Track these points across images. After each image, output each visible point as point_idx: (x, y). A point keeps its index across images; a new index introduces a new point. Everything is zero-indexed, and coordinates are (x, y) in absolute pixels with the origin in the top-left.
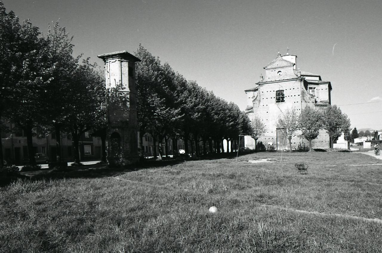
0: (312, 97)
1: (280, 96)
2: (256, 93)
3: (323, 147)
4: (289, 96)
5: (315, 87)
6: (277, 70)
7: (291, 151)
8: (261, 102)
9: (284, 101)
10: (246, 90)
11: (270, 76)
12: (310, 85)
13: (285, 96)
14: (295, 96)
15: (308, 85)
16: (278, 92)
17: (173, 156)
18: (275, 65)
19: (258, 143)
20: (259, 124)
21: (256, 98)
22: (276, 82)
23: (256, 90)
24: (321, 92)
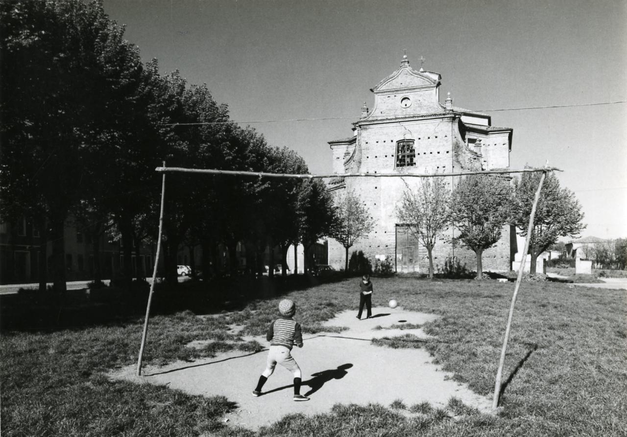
0: (475, 159)
1: (404, 152)
2: (351, 149)
3: (497, 268)
4: (425, 153)
5: (480, 139)
6: (400, 96)
7: (431, 276)
8: (362, 164)
9: (415, 164)
10: (330, 141)
11: (383, 107)
12: (471, 133)
13: (416, 153)
14: (439, 153)
15: (467, 133)
16: (402, 144)
17: (38, 285)
18: (395, 84)
19: (354, 254)
20: (355, 211)
21: (352, 156)
22: (397, 120)
23: (352, 142)
24: (493, 150)
